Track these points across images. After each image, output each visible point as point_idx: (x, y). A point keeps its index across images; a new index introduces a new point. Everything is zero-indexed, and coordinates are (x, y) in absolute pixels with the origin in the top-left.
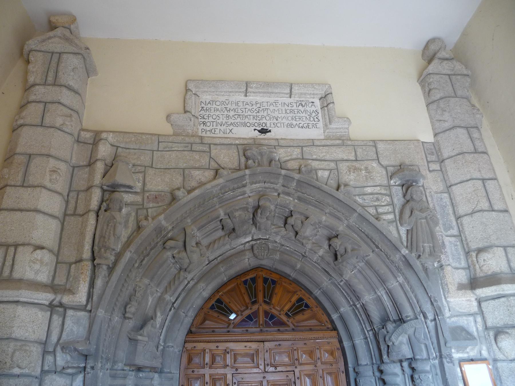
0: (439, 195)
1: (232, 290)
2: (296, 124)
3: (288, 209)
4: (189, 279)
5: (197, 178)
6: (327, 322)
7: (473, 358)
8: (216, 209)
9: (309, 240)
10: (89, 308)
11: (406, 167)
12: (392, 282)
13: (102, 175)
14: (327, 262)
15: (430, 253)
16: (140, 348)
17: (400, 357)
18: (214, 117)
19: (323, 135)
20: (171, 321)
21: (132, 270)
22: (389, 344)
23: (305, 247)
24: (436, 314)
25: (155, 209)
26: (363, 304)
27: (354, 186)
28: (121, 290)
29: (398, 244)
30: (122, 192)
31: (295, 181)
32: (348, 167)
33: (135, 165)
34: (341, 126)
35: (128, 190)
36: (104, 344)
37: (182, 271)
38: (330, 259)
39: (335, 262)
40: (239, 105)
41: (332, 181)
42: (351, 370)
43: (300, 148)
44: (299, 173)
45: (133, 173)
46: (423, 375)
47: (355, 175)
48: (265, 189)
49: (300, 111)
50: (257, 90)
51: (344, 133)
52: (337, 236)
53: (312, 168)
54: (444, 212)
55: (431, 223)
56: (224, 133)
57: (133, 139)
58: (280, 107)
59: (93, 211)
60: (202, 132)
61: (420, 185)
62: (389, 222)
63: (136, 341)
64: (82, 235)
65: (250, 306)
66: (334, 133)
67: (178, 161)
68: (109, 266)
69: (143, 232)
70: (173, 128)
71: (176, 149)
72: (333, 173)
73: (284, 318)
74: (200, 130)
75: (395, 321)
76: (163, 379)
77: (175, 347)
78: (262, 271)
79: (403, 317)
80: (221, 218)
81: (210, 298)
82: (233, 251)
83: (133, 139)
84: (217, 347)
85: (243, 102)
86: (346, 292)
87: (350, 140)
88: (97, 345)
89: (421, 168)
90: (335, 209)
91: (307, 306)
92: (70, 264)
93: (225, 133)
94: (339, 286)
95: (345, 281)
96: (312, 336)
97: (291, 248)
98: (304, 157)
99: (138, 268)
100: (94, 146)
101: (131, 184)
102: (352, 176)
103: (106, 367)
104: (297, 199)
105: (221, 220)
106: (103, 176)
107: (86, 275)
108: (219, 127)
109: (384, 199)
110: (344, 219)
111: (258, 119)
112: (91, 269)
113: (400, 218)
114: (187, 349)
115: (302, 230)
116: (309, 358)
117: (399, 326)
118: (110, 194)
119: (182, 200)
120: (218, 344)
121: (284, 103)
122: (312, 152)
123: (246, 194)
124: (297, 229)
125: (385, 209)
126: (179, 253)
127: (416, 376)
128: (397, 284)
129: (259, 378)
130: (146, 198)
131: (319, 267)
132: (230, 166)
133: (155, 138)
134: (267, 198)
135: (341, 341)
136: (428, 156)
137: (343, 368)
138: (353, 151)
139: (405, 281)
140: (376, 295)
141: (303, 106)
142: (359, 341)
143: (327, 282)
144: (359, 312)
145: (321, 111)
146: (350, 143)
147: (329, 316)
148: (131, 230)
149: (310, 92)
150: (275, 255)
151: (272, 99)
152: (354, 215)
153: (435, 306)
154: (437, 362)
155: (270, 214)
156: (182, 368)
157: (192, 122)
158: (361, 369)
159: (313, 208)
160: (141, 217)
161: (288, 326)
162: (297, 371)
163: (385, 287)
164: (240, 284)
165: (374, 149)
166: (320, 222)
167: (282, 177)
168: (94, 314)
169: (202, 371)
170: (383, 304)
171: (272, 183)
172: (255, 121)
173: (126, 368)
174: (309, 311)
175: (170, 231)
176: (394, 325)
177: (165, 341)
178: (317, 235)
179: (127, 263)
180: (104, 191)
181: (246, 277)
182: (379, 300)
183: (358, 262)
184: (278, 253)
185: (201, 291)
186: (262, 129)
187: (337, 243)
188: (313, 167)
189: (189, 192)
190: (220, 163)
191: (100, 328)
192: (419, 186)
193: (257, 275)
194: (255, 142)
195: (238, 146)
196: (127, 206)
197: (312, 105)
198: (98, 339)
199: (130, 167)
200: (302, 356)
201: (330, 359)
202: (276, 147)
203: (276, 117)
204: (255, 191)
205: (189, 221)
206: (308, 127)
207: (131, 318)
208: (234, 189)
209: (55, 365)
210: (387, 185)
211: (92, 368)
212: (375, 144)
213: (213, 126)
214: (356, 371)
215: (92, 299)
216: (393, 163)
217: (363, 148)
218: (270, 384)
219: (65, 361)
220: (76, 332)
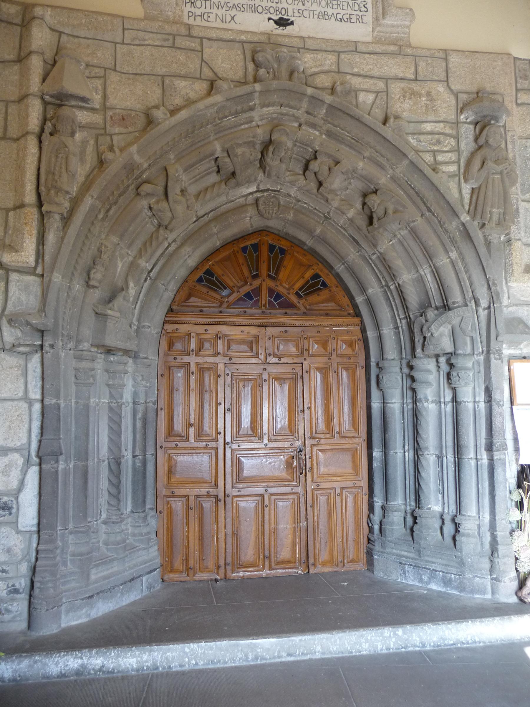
0: (523, 141)
1: (227, 259)
2: (333, 14)
3: (311, 148)
4: (170, 240)
5: (183, 92)
6: (348, 305)
7: (526, 356)
8: (209, 143)
9: (337, 195)
10: (39, 271)
11: (485, 95)
12: (441, 258)
13: (41, 77)
14: (357, 227)
15: (499, 222)
16: (110, 324)
17: (438, 351)
20: (147, 295)
21: (95, 222)
22: (427, 336)
23: (330, 204)
24: (491, 301)
25: (123, 135)
26: (399, 284)
27: (408, 120)
28: (81, 249)
29: (458, 208)
31: (325, 106)
32: (403, 89)
34: (399, 23)
36: (64, 319)
37: (161, 228)
38: (362, 222)
39: (369, 228)
41: (377, 110)
42: (373, 364)
43: (337, 54)
44: (332, 94)
45: (88, 77)
46: (463, 372)
47: (412, 103)
48: (280, 116)
51: (403, 35)
52: (375, 192)
53: (351, 87)
54: (526, 166)
55: (507, 180)
56: (223, 22)
57: (84, 21)
59: (33, 133)
60: (189, 16)
62: (449, 176)
63: (105, 316)
64: (20, 168)
65: (249, 280)
66: (387, 33)
67: (154, 63)
68: (62, 215)
69: (108, 169)
70: (143, 7)
71: (150, 42)
73: (294, 299)
74: (186, 13)
75: (437, 308)
76: (139, 366)
77: (152, 328)
78: (267, 235)
79: (449, 303)
80: (216, 156)
81: (196, 268)
82: (230, 204)
83: (84, 21)
84: (206, 330)
87: (410, 46)
88: (56, 319)
89: (505, 99)
90: (377, 152)
91: (324, 284)
92: (8, 210)
93: (224, 21)
94: (370, 260)
95: (379, 254)
96: (328, 323)
97: (310, 205)
98: (342, 70)
99: (103, 220)
100: (24, 29)
101: (86, 94)
102: (407, 105)
103: (69, 346)
104: (325, 134)
105: (216, 159)
106: (42, 80)
107: (31, 226)
108: (215, 10)
109: (447, 142)
110: (388, 167)
112: (37, 219)
113: (465, 172)
114: (167, 331)
115: (328, 180)
116: (322, 349)
117: (442, 314)
118: (55, 110)
119: (163, 124)
120: (206, 327)
122: (353, 63)
123: (253, 121)
124: (321, 178)
125: (447, 157)
126: (158, 202)
127: (454, 373)
128: (448, 260)
129: (258, 369)
130: (108, 118)
131: (346, 234)
132: (232, 76)
133: (117, 22)
134: (284, 129)
135: (363, 331)
136: (519, 81)
137: (362, 362)
138: (414, 64)
139: (460, 257)
140: (418, 274)
142: (388, 331)
143: (354, 254)
144: (392, 295)
146: (410, 52)
147: (352, 298)
148: (89, 165)
152: (404, 163)
153: (493, 290)
154: (482, 358)
155: (286, 153)
156: (161, 354)
158: (386, 364)
159: (347, 149)
160: (103, 148)
161: (299, 309)
162: (305, 363)
163: (432, 264)
164: (238, 252)
165: (444, 64)
166: (355, 171)
167: (306, 99)
168: (48, 279)
169: (186, 359)
170: (425, 286)
171: (291, 107)
173: (92, 350)
174: (327, 291)
175: (146, 170)
176: (436, 312)
177: (139, 320)
178: (348, 188)
179: (87, 213)
180: (45, 104)
181: (245, 242)
182: (421, 280)
183: (400, 229)
184: (292, 212)
185: (186, 257)
186: (281, 18)
187: (374, 201)
188: (353, 87)
189: (173, 112)
190: (216, 70)
191: (58, 298)
192: (500, 126)
193: (260, 240)
194: (269, 39)
195: (245, 45)
196: (81, 129)
198: (56, 310)
199: (82, 67)
200: (313, 346)
201: (349, 351)
202: (301, 50)
204: (267, 119)
205: (172, 156)
207: (96, 287)
208: (236, 113)
209: (3, 342)
210: (455, 121)
211: (52, 346)
212: (446, 56)
213: (206, 8)
214: (380, 366)
215: (43, 260)
216: (467, 88)
217: (427, 61)
218: (271, 377)
219: (14, 338)
220: (25, 302)
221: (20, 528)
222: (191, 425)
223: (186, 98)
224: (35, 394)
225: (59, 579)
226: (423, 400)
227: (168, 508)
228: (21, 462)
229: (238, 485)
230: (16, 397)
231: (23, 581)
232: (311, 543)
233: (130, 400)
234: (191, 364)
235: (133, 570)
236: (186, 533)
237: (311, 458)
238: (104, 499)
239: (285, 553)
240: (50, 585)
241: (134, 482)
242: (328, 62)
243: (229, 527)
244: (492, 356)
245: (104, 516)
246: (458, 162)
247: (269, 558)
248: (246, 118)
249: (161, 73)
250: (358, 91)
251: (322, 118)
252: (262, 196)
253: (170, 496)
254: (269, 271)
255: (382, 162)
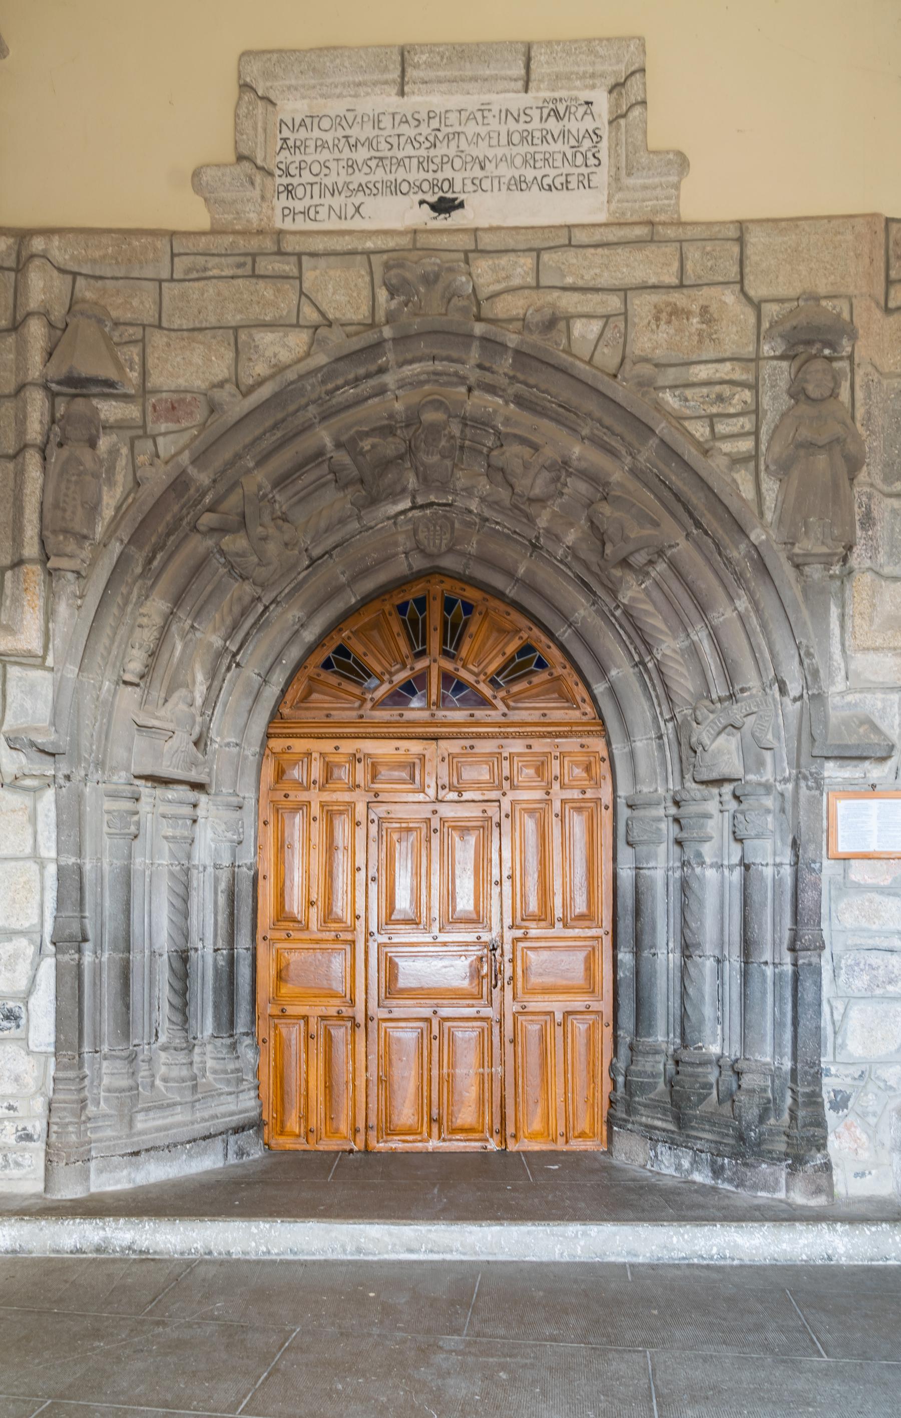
1: (375, 625)
2: (535, 178)
4: (266, 601)
5: (269, 353)
10: (50, 662)
12: (721, 610)
18: (316, 168)
19: (606, 209)
30: (95, 396)
32: (655, 307)
33: (121, 324)
35: (107, 390)
40: (382, 125)
41: (606, 350)
43: (534, 254)
47: (672, 331)
49: (549, 137)
50: (431, 74)
51: (666, 202)
56: (340, 218)
57: (110, 250)
58: (494, 124)
60: (284, 216)
61: (844, 354)
71: (215, 272)
72: (612, 326)
73: (486, 690)
74: (278, 212)
83: (110, 250)
85: (393, 114)
86: (626, 632)
91: (541, 664)
99: (142, 575)
101: (110, 373)
102: (664, 334)
110: (624, 453)
111: (433, 167)
120: (337, 742)
121: (507, 111)
122: (563, 267)
129: (425, 812)
130: (150, 409)
132: (351, 315)
133: (162, 244)
138: (678, 256)
141: (559, 117)
144: (651, 679)
145: (610, 132)
149: (582, 69)
150: (468, 544)
151: (471, 101)
152: (651, 442)
154: (790, 786)
157: (258, 188)
159: (552, 425)
165: (736, 249)
166: (566, 463)
167: (476, 344)
169: (303, 796)
172: (423, 175)
180: (53, 396)
182: (694, 651)
186: (441, 199)
189: (246, 393)
190: (324, 307)
196: (108, 431)
197: (585, 113)
199: (107, 329)
203: (481, 158)
206: (566, 185)
210: (753, 356)
216: (782, 291)
221: (32, 1047)
222: (312, 903)
223: (273, 361)
224: (49, 851)
225: (84, 1122)
226: (693, 862)
227: (276, 1035)
228: (31, 950)
229: (387, 1002)
230: (21, 855)
231: (37, 1124)
232: (510, 1102)
233: (209, 862)
234: (313, 804)
235: (208, 1124)
236: (304, 1075)
237: (512, 961)
238: (164, 1014)
239: (466, 1116)
240: (71, 1129)
241: (217, 991)
242: (519, 270)
243: (373, 1068)
244: (803, 784)
245: (163, 1039)
246: (756, 433)
247: (439, 1121)
248: (373, 387)
249: (233, 324)
250: (572, 317)
251: (505, 374)
252: (423, 516)
253: (279, 1017)
254: (445, 643)
255: (613, 443)
